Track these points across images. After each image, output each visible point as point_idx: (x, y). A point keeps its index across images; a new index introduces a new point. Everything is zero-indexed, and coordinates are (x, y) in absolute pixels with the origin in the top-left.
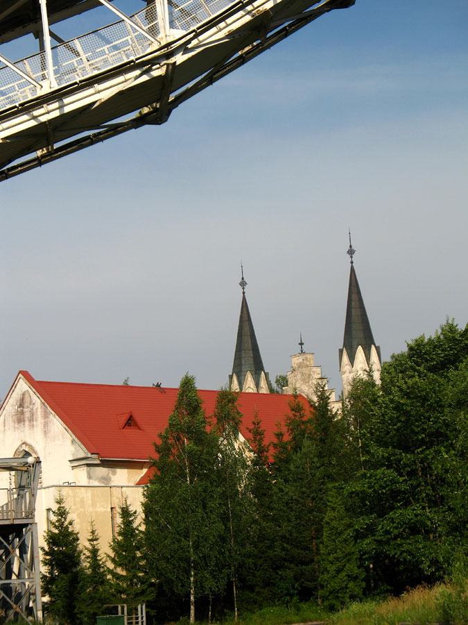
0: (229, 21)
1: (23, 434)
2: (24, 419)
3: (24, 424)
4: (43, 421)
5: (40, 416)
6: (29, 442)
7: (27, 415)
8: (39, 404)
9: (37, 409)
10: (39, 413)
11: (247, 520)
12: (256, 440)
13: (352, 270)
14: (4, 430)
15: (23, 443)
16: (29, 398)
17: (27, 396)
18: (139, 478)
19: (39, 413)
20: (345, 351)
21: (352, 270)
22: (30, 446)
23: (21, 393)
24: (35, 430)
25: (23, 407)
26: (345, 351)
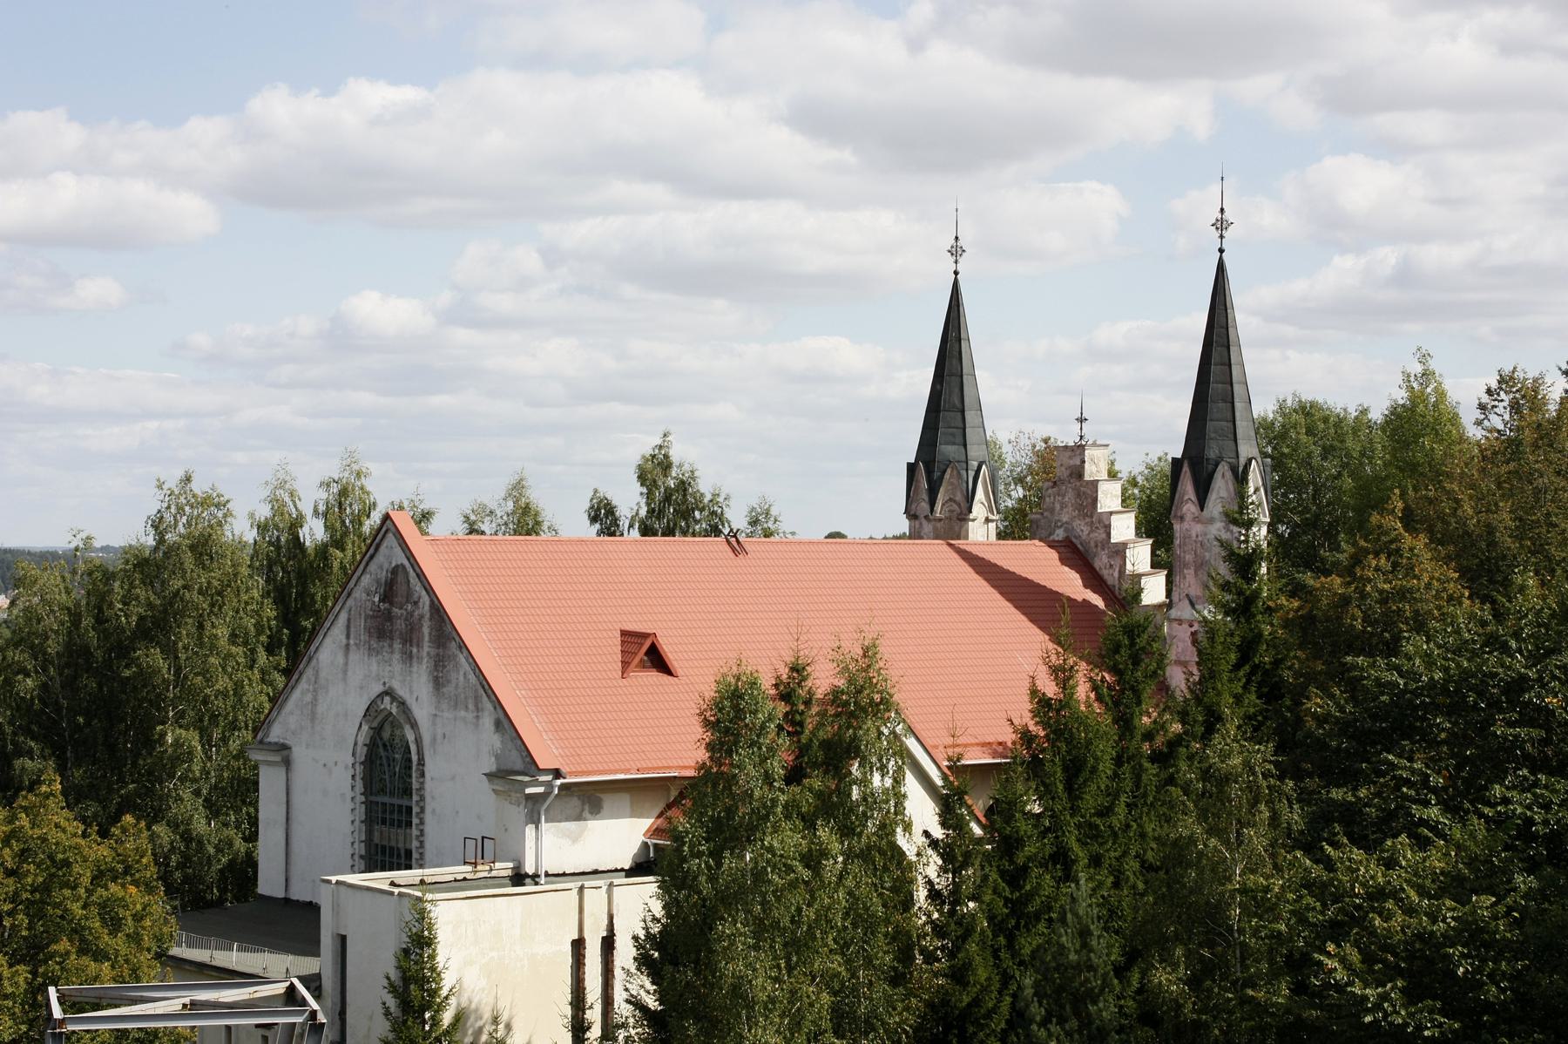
0: (451, 878)
1: (388, 668)
2: (391, 631)
3: (391, 646)
4: (433, 652)
5: (427, 638)
6: (402, 692)
7: (400, 625)
8: (427, 608)
9: (422, 617)
10: (426, 630)
11: (1496, 931)
12: (1438, 517)
13: (1221, 267)
14: (347, 646)
15: (386, 693)
16: (404, 587)
17: (400, 578)
18: (1177, 535)
19: (426, 630)
20: (1186, 468)
21: (1221, 267)
22: (402, 704)
23: (383, 575)
24: (415, 669)
25: (391, 604)
26: (1186, 468)
